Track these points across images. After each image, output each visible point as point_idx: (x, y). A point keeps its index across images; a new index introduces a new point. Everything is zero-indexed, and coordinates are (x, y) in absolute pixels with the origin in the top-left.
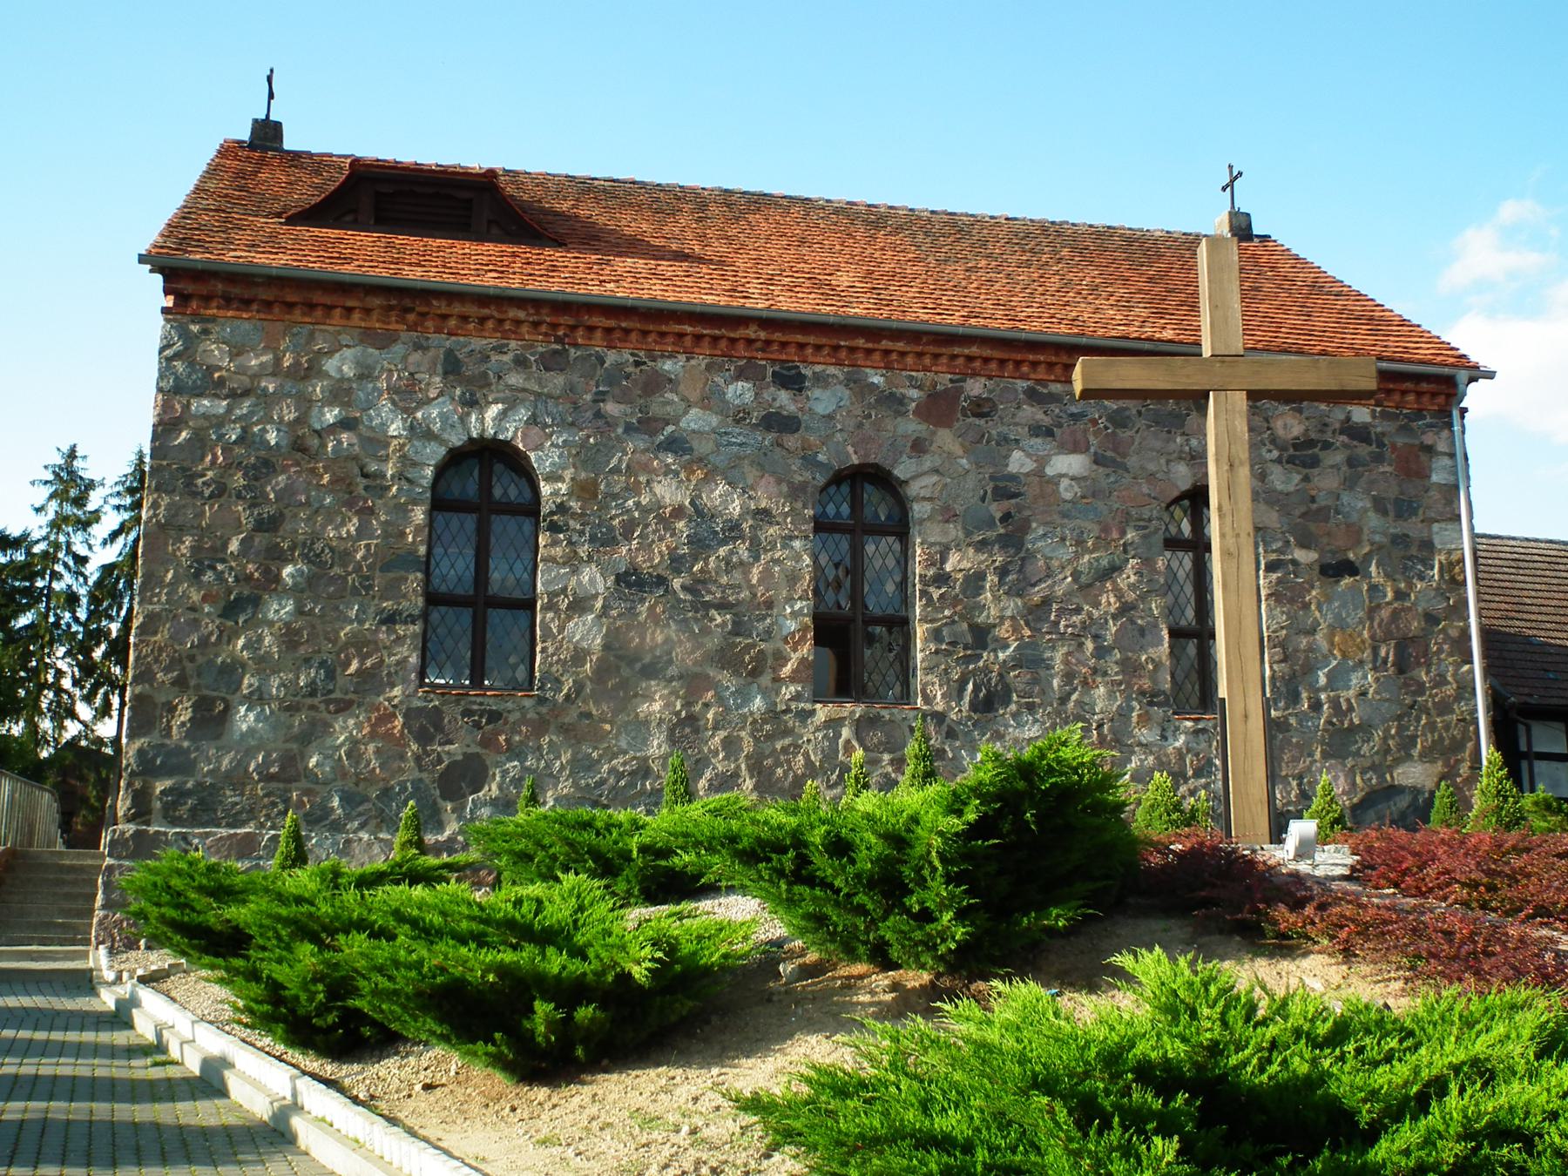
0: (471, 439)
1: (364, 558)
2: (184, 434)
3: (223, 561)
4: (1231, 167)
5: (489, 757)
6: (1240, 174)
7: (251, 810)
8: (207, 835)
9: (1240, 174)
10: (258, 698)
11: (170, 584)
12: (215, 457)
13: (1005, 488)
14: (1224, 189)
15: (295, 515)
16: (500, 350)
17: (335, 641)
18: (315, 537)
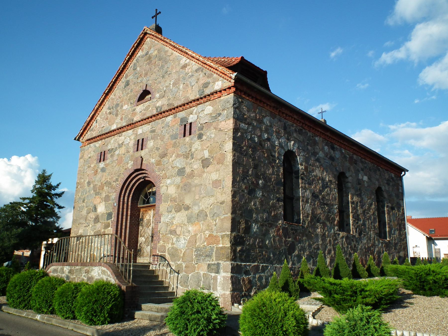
0: (288, 150)
1: (274, 181)
2: (239, 134)
3: (248, 177)
4: (156, 10)
5: (296, 243)
6: (160, 12)
7: (256, 258)
8: (250, 265)
9: (160, 12)
10: (256, 222)
11: (238, 182)
12: (246, 143)
13: (358, 180)
14: (153, 18)
15: (261, 165)
16: (292, 125)
17: (269, 205)
18: (265, 172)
